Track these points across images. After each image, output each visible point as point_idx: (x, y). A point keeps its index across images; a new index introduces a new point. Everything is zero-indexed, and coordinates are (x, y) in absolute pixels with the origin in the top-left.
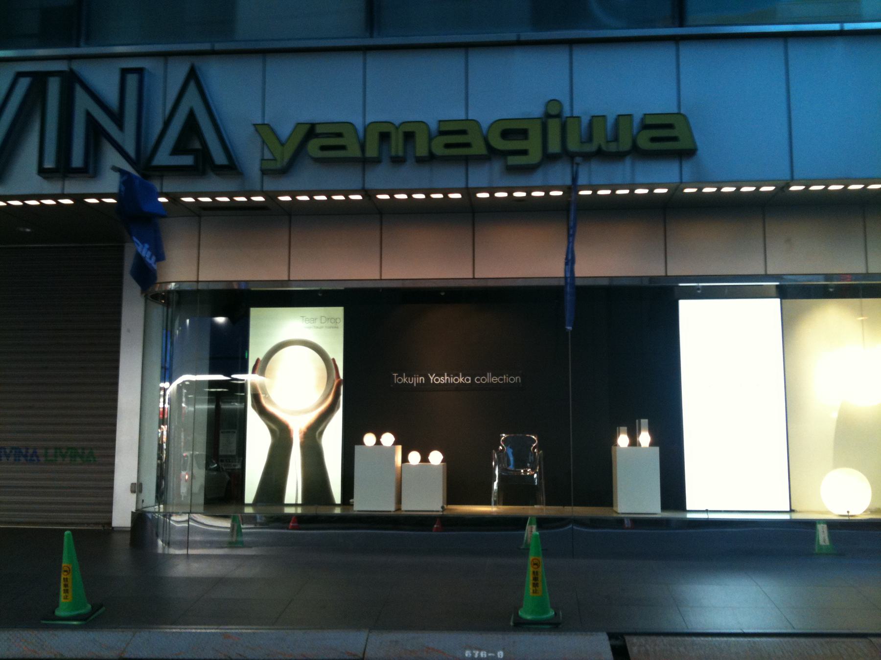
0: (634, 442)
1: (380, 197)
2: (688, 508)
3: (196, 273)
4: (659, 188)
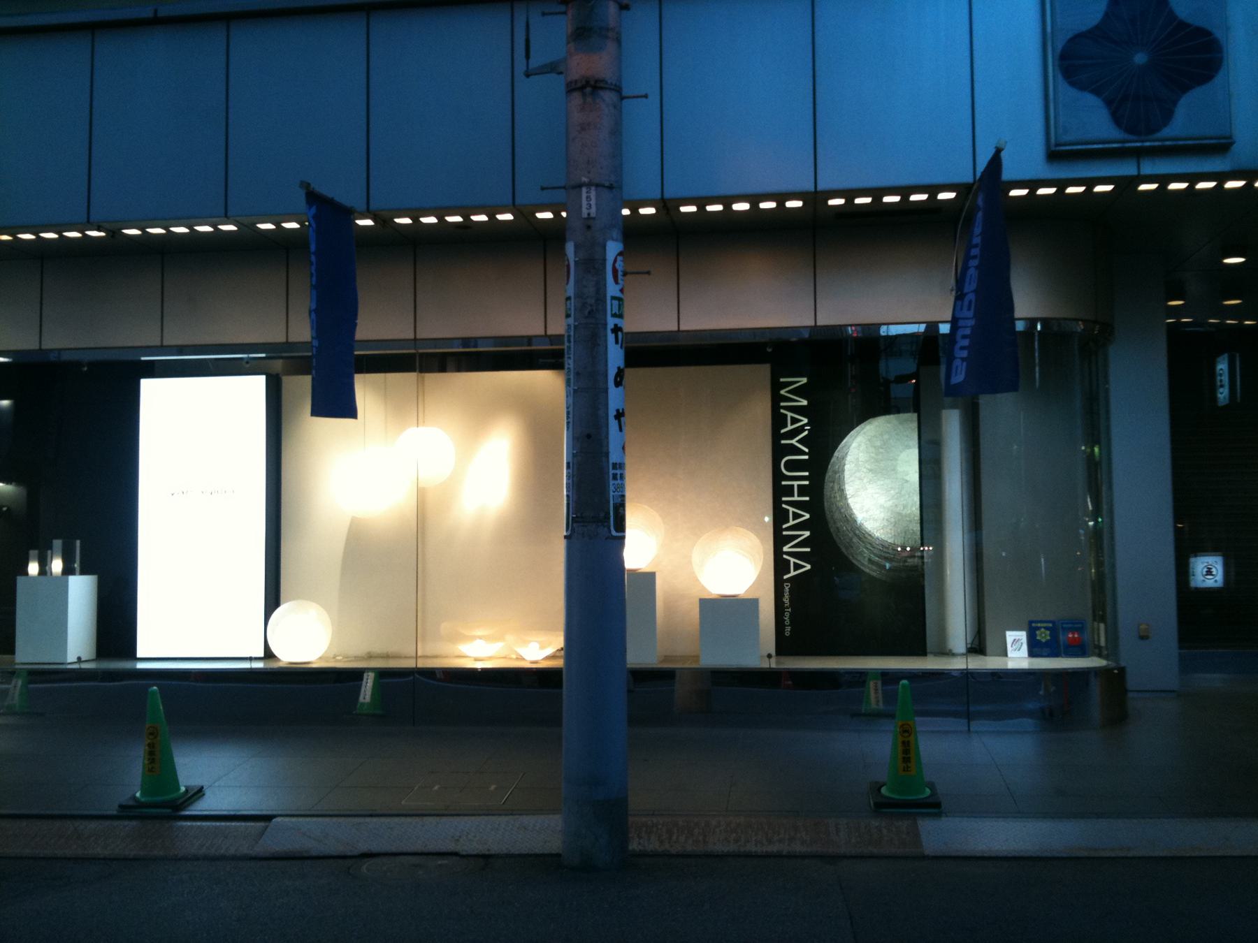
0: (44, 570)
1: (684, 209)
2: (139, 655)
3: (37, 338)
4: (644, 206)
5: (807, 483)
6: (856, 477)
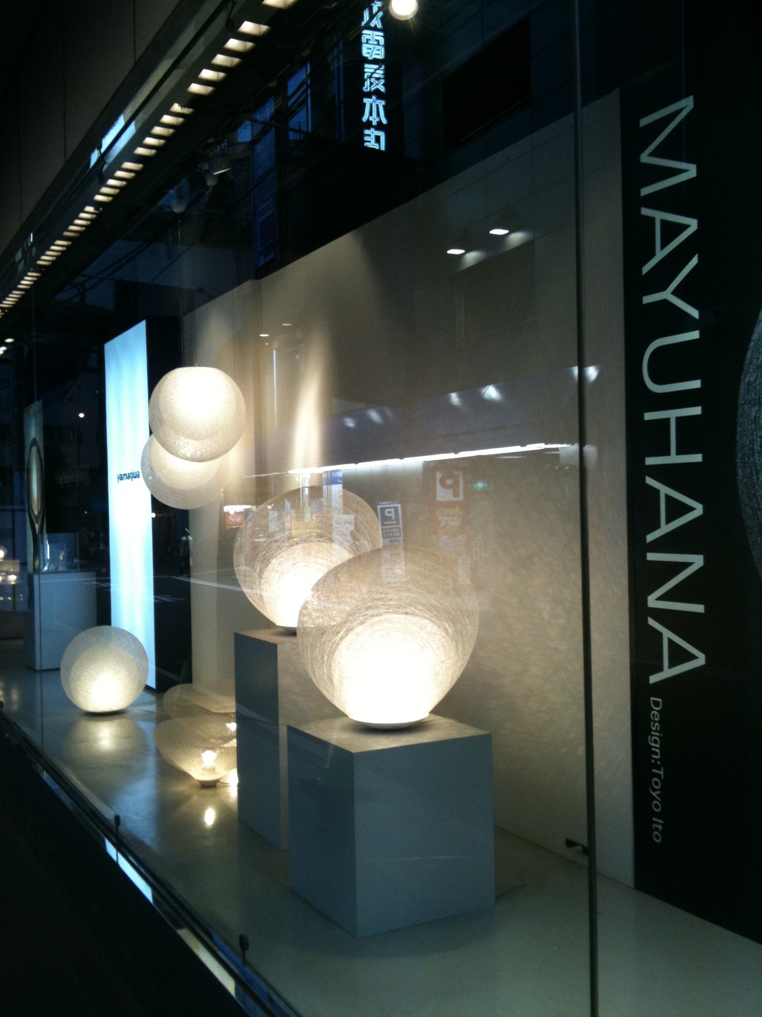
5: (697, 411)
6: (751, 372)
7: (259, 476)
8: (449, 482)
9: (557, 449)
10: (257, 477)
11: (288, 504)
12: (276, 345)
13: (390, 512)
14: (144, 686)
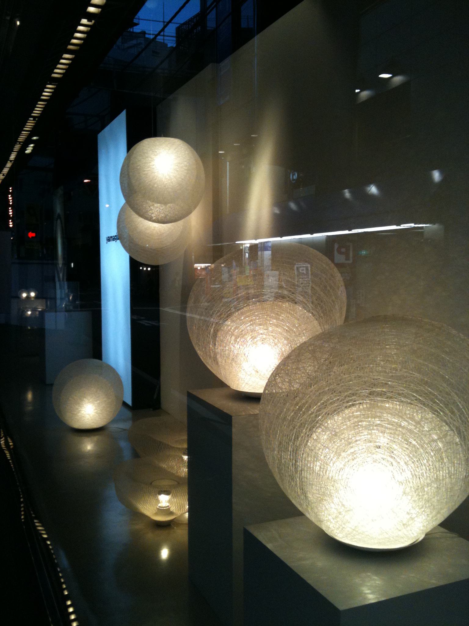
7: (215, 245)
8: (343, 250)
9: (422, 228)
10: (213, 246)
11: (234, 264)
12: (229, 158)
13: (303, 270)
14: (122, 402)
